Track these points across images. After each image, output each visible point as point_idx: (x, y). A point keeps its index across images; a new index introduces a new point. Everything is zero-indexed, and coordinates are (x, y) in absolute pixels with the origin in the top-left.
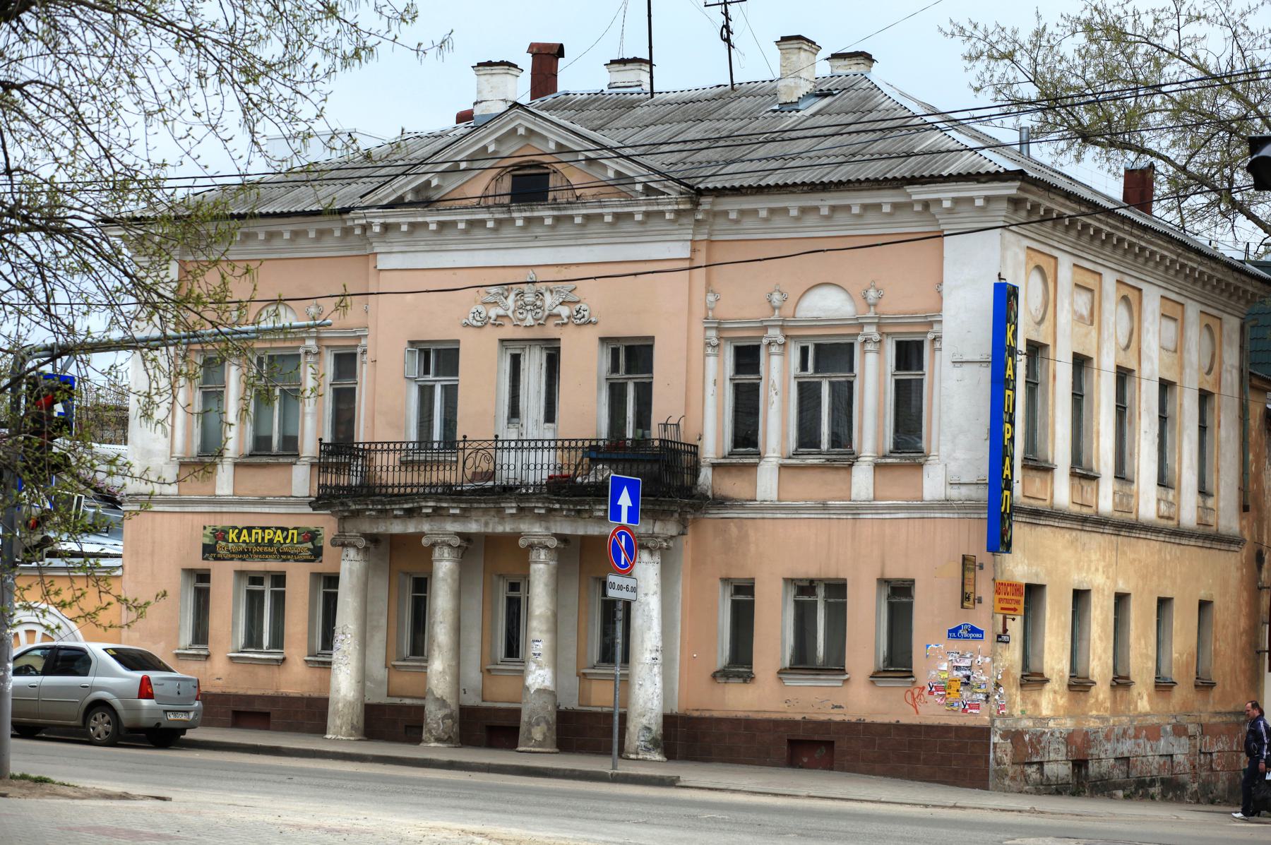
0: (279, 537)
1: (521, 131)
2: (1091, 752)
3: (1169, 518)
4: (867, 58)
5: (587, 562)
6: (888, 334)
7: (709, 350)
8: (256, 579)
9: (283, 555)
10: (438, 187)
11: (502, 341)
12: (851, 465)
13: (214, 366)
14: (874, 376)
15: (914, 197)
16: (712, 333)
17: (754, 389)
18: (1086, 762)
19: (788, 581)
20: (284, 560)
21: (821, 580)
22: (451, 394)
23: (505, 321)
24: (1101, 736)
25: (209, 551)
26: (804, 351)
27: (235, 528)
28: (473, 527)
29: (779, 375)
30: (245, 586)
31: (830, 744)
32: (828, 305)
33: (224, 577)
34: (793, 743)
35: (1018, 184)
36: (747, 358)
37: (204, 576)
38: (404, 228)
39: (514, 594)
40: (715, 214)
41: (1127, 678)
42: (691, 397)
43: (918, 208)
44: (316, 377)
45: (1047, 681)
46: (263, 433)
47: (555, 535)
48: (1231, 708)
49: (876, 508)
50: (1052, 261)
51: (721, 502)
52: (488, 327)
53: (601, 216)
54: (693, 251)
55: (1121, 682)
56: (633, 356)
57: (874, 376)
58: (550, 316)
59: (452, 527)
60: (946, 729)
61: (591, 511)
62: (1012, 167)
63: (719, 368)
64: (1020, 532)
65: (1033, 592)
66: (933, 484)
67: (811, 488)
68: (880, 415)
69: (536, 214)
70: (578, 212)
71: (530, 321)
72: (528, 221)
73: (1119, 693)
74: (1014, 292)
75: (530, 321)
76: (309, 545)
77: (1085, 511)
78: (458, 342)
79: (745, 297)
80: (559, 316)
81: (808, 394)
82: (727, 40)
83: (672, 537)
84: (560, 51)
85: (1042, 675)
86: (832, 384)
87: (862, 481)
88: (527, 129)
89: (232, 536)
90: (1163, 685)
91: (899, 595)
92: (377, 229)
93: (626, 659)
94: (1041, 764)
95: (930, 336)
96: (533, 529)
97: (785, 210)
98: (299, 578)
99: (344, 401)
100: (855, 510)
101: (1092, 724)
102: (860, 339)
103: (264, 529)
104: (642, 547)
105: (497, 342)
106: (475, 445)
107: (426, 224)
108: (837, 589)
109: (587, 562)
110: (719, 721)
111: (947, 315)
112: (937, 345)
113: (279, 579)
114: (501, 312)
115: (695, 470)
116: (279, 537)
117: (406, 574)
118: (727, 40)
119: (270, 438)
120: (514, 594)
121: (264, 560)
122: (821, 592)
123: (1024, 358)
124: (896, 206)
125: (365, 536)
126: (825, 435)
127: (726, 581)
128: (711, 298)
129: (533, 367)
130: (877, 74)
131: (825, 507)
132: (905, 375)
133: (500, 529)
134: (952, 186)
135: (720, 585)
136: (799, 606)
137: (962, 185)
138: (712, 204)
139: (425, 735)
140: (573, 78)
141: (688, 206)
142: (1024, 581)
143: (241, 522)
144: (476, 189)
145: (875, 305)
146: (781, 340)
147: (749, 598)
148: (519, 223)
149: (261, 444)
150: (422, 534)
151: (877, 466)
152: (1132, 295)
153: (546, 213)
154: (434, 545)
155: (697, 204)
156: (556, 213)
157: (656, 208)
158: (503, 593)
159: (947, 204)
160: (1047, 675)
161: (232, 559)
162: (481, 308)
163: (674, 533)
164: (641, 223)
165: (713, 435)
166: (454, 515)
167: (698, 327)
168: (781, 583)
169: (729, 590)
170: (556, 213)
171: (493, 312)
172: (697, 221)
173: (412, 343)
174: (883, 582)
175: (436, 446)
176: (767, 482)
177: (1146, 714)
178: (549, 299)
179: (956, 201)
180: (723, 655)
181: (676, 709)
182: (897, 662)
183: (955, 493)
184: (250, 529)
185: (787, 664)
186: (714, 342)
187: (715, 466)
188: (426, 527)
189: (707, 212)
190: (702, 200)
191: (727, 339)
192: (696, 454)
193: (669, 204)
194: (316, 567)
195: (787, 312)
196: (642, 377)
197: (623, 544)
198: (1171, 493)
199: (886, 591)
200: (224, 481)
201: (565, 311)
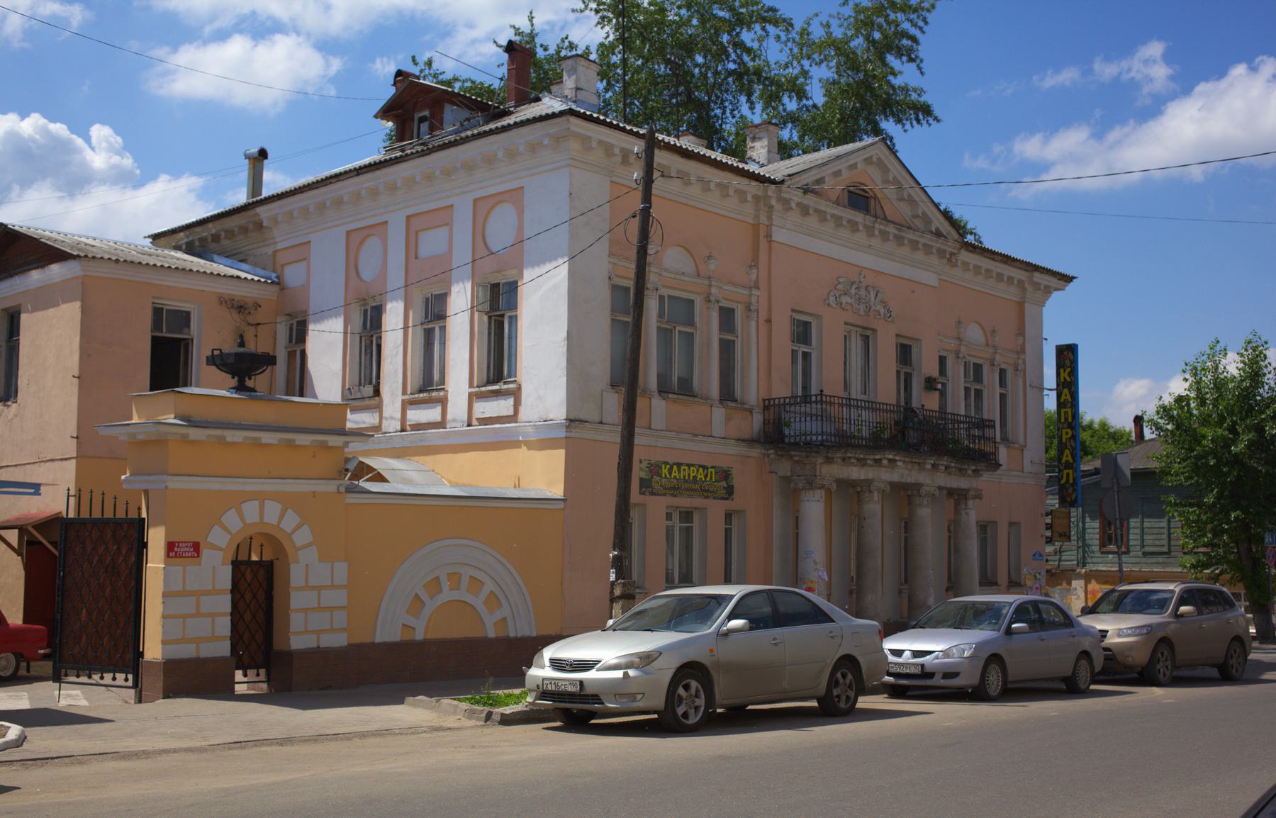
0: (701, 476)
2: (1170, 448)
20: (707, 497)
27: (666, 463)
62: (564, 107)
74: (37, 493)
76: (724, 484)
89: (665, 471)
121: (691, 496)
123: (1046, 385)
129: (856, 345)
161: (664, 495)
175: (813, 399)
184: (679, 465)
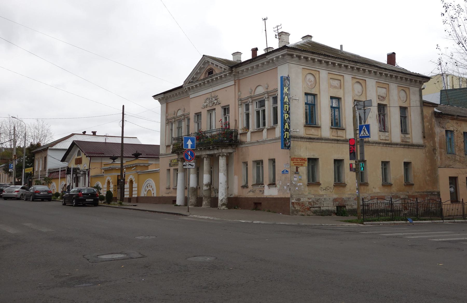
4: (311, 36)
5: (214, 159)
18: (345, 206)
30: (176, 172)
31: (261, 203)
32: (260, 90)
34: (256, 204)
37: (169, 170)
41: (367, 183)
48: (425, 190)
50: (318, 72)
51: (242, 143)
54: (235, 82)
56: (226, 110)
63: (242, 110)
64: (293, 143)
67: (256, 138)
68: (269, 117)
73: (362, 187)
78: (201, 112)
79: (245, 94)
81: (258, 113)
84: (256, 49)
100: (264, 142)
108: (262, 161)
110: (242, 198)
115: (236, 137)
130: (314, 40)
131: (258, 142)
140: (259, 53)
142: (307, 157)
160: (321, 182)
165: (241, 126)
173: (196, 114)
176: (248, 138)
177: (378, 193)
178: (213, 99)
187: (241, 134)
190: (233, 69)
195: (252, 95)
196: (263, 108)
198: (387, 134)
201: (215, 101)
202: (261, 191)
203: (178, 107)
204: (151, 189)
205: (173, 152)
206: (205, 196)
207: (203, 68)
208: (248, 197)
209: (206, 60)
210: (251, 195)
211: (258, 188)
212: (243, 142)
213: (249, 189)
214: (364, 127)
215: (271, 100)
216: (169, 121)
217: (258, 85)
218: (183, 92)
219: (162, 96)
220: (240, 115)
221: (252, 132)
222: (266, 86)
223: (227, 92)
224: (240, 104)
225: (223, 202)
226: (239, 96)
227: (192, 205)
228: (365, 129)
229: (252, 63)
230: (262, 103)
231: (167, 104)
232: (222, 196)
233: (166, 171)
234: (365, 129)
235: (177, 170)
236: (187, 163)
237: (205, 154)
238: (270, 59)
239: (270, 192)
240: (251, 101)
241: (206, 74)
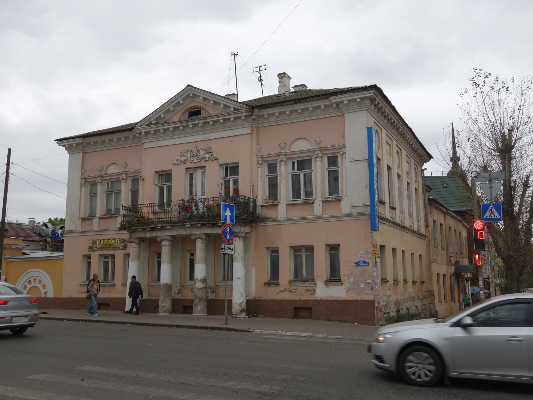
0: (113, 242)
1: (191, 95)
3: (411, 227)
6: (324, 154)
7: (259, 166)
8: (106, 257)
9: (115, 248)
10: (163, 118)
11: (186, 169)
12: (313, 203)
13: (94, 185)
14: (319, 171)
15: (333, 101)
16: (260, 159)
17: (276, 178)
19: (291, 247)
21: (303, 246)
22: (169, 188)
23: (187, 161)
24: (402, 301)
25: (91, 248)
26: (293, 163)
28: (175, 233)
29: (285, 172)
30: (103, 259)
31: (310, 309)
32: (301, 146)
33: (95, 256)
34: (296, 309)
35: (374, 91)
36: (272, 168)
37: (89, 257)
38: (152, 132)
39: (192, 257)
40: (259, 117)
42: (253, 184)
43: (334, 106)
44: (125, 188)
45: (388, 281)
46: (110, 208)
47: (205, 234)
49: (323, 218)
51: (266, 219)
52: (182, 164)
53: (219, 120)
54: (252, 131)
55: (405, 282)
56: (232, 169)
57: (319, 171)
58: (202, 158)
59: (168, 233)
60: (357, 301)
61: (216, 224)
63: (263, 172)
65: (382, 247)
66: (345, 207)
67: (297, 213)
68: (323, 184)
69: (196, 122)
70: (211, 121)
71: (195, 161)
72: (194, 125)
75: (195, 161)
76: (123, 244)
77: (393, 220)
78: (171, 170)
79: (270, 149)
80: (205, 158)
81: (296, 179)
82: (261, 81)
83: (247, 233)
85: (386, 279)
86: (305, 174)
87: (318, 208)
88: (193, 94)
89: (98, 243)
90: (414, 283)
91: (334, 249)
92: (143, 134)
93: (232, 279)
94: (388, 313)
95: (341, 153)
96: (197, 232)
97: (285, 112)
98: (119, 255)
99: (135, 194)
100: (316, 219)
101: (400, 297)
102: (314, 156)
103: (108, 239)
104: (236, 236)
105: (184, 169)
106: (175, 202)
107: (159, 130)
108: (310, 249)
109: (214, 242)
110: (265, 301)
111: (347, 145)
112: (344, 156)
113: (113, 256)
114: (186, 158)
115: (255, 208)
116: (113, 242)
117: (156, 252)
118: (261, 81)
119: (111, 210)
120: (192, 257)
121: (108, 250)
122: (303, 251)
124: (326, 106)
125: (138, 238)
126: (302, 191)
127: (268, 248)
128: (259, 147)
131: (304, 218)
132: (332, 169)
133: (184, 233)
134: (348, 95)
135: (265, 249)
136: (296, 257)
137: (352, 94)
138: (258, 112)
139: (159, 310)
141: (250, 113)
143: (101, 238)
144: (176, 118)
145: (319, 144)
146: (285, 159)
147: (277, 254)
148: (191, 126)
149: (109, 211)
150: (158, 237)
151: (323, 202)
152: (399, 151)
153: (200, 122)
154: (162, 240)
155: (253, 112)
156: (203, 121)
157: (238, 115)
158: (188, 256)
159: (346, 102)
162: (179, 158)
163: (248, 231)
164: (233, 122)
165: (261, 195)
166: (168, 229)
167: (255, 158)
168: (288, 248)
169: (269, 252)
170: (203, 121)
171: (183, 159)
172: (253, 119)
173: (156, 172)
174: (327, 245)
176: (281, 211)
178: (202, 152)
179: (349, 101)
180: (267, 277)
181: (250, 297)
182: (334, 277)
183: (354, 211)
184: (104, 240)
185: (292, 279)
186: (261, 162)
187: (262, 206)
188: (159, 234)
189: (257, 116)
190: (255, 111)
191: (265, 161)
192: (255, 203)
193: (243, 113)
194: (125, 252)
195: (287, 150)
196: (235, 177)
197: (228, 236)
199: (329, 249)
200: (96, 223)
202: (308, 290)
203: (112, 162)
204: (40, 286)
205: (122, 228)
206: (199, 298)
207: (182, 104)
208: (280, 299)
209: (190, 92)
210: (286, 296)
211: (300, 287)
212: (267, 218)
213: (281, 288)
214: (492, 206)
215: (130, 181)
216: (87, 183)
217: (299, 137)
218: (135, 136)
219: (80, 141)
220: (259, 179)
221: (100, 218)
222: (124, 165)
223: (237, 145)
224: (83, 183)
225: (243, 307)
226: (258, 151)
227: (166, 311)
228: (494, 210)
229: (321, 101)
230: (303, 164)
231: (84, 154)
232: (238, 298)
233: (80, 259)
234: (494, 210)
235: (128, 255)
236: (226, 246)
237: (199, 232)
238: (334, 103)
239: (323, 292)
240: (100, 181)
241: (184, 113)
